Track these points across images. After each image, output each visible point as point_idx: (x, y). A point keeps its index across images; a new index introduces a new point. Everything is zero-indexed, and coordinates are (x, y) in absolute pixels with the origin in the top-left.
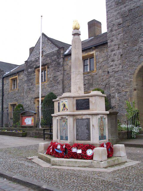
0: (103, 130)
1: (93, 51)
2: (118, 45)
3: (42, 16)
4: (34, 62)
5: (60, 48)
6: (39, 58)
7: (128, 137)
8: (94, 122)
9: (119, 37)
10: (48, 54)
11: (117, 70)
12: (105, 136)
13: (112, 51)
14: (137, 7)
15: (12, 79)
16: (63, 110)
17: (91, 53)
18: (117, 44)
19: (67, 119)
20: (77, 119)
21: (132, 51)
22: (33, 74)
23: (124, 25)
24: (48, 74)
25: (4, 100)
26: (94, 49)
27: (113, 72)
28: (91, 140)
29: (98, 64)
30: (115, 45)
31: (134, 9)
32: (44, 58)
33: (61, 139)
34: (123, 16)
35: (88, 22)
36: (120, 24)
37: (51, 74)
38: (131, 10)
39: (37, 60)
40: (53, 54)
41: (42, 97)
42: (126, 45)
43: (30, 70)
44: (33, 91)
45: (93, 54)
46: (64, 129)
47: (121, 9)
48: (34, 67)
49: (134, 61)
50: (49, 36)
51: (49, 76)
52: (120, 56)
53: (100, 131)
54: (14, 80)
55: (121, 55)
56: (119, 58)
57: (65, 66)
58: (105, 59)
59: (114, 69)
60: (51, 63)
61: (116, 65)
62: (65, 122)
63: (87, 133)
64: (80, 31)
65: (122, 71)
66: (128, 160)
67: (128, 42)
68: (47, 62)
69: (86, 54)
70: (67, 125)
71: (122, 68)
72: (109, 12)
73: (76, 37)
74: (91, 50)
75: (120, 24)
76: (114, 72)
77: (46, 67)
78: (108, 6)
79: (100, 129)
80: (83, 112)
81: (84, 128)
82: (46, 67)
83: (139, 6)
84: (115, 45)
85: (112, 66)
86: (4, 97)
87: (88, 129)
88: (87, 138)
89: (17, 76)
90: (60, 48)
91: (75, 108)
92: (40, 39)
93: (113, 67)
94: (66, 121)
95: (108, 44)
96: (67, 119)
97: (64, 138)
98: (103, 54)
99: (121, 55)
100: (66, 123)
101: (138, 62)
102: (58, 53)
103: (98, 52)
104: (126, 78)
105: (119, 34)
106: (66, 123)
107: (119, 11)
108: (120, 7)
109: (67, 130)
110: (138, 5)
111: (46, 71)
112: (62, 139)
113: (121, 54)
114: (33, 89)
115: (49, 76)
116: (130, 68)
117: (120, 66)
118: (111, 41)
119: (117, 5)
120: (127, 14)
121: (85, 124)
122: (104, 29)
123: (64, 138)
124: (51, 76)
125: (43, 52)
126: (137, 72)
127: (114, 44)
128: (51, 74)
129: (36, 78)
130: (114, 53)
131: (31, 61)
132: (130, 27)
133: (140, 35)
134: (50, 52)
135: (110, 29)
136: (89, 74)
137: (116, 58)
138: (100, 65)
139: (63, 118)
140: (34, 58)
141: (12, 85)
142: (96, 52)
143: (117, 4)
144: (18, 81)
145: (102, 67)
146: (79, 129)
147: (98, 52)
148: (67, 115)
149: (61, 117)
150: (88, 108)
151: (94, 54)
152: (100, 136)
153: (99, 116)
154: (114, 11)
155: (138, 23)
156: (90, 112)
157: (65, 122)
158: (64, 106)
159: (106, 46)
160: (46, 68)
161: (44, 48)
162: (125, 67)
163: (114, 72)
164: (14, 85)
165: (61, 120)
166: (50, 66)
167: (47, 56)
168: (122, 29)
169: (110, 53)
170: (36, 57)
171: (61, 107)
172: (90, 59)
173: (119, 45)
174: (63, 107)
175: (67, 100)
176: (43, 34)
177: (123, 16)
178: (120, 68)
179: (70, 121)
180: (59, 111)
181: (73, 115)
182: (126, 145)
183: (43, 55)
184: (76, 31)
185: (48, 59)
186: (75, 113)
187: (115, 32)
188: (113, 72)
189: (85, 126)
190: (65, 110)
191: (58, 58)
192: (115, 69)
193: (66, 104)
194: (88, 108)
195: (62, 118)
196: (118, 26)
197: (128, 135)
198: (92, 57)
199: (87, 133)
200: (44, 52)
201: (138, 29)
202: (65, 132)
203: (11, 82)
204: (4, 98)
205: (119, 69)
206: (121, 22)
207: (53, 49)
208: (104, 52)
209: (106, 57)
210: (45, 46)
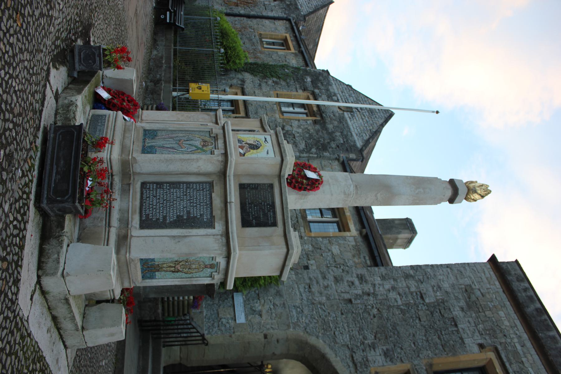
0: (173, 269)
1: (357, 230)
2: (373, 293)
3: (437, 112)
4: (328, 90)
5: (361, 151)
6: (338, 101)
7: (146, 321)
8: (202, 243)
9: (393, 295)
10: (347, 123)
11: (315, 288)
12: (152, 277)
13: (361, 278)
14: (461, 338)
15: (286, 40)
16: (240, 141)
17: (352, 226)
18: (377, 288)
19: (212, 153)
20: (211, 184)
21: (361, 329)
22: (298, 86)
23: (420, 308)
24: (299, 120)
25: (239, 18)
26: (361, 233)
27: (310, 279)
28: (142, 231)
29: (326, 241)
30: (374, 285)
31: (458, 331)
32: (337, 115)
33: (145, 130)
34: (441, 306)
35: (411, 220)
36: (422, 297)
37: (299, 127)
38: (456, 325)
39: (330, 97)
40: (346, 135)
41: (245, 101)
42: (375, 311)
43: (309, 79)
44: (260, 85)
45: (349, 230)
46: (180, 140)
47: (457, 298)
48: (317, 91)
49: (336, 333)
50: (386, 130)
51: (295, 124)
52: (347, 296)
53: (172, 262)
54: (284, 44)
55: (350, 301)
56: (343, 295)
57: (319, 162)
58: (339, 261)
59: (317, 283)
60: (327, 129)
61: (326, 287)
62: (204, 146)
63: (165, 218)
64: (460, 202)
65: (313, 304)
66: (72, 353)
67: (381, 318)
68: (328, 120)
69: (348, 214)
70: (192, 152)
71: (320, 303)
72: (449, 270)
73: (449, 193)
74: (358, 226)
75: (422, 297)
76: (308, 281)
77: (318, 118)
78: (462, 269)
79: (177, 262)
80: (233, 205)
81: (180, 207)
82: (318, 118)
83: (464, 343)
84: (374, 285)
85: (324, 278)
86: (245, 19)
87: (181, 222)
88: (147, 215)
89: (293, 50)
90: (361, 151)
91: (246, 181)
92: (378, 104)
93: (321, 281)
94: (205, 148)
95: (376, 269)
96: (212, 153)
97: (150, 143)
98: (348, 255)
99: (350, 301)
100: (198, 148)
101: (336, 342)
102: (350, 147)
103: (354, 243)
104: (294, 313)
105: (399, 294)
106: (200, 150)
107: (452, 296)
108: (460, 297)
109: (174, 153)
110: (467, 341)
111: (307, 116)
112: (145, 135)
113: (353, 300)
114: (263, 85)
115: (296, 122)
116: (320, 323)
117: (324, 298)
118: (382, 275)
119: (464, 290)
120: (446, 315)
121: (195, 213)
122: (399, 257)
123: (150, 143)
124: (295, 129)
125: (350, 110)
126: (312, 340)
127: (376, 282)
128: (299, 127)
129: (288, 93)
130: (357, 282)
131: (329, 84)
132: (417, 321)
133: (399, 347)
134: (351, 127)
135: (412, 272)
136: (300, 220)
137: (343, 286)
138: (323, 248)
139: (215, 140)
140: (336, 91)
141: (274, 39)
142: (354, 237)
143: (466, 291)
144: (281, 53)
145: (319, 250)
146: (177, 193)
147: (354, 243)
148: (226, 155)
149: (221, 136)
150: (246, 223)
151: (347, 234)
152: (153, 260)
153: (222, 262)
154: (451, 283)
155: (427, 341)
156: (235, 228)
157: (204, 146)
158: (255, 147)
159: (368, 262)
160: (314, 118)
161: (359, 116)
162: (321, 308)
163: (308, 281)
164: (273, 44)
165: (208, 135)
166: (318, 127)
167: (341, 120)
168: (412, 302)
169: (354, 271)
170: (338, 95)
171: (249, 138)
172: (337, 223)
173: (375, 295)
174: (249, 142)
175: (271, 154)
176: (388, 115)
177: (441, 304)
178: (318, 298)
179: (205, 163)
180: (233, 130)
181: (223, 174)
182: (121, 345)
183: (344, 111)
184: (462, 191)
185: (336, 123)
186: (232, 178)
187: (405, 285)
188: (310, 279)
189: (188, 213)
190: (242, 147)
191: (338, 146)
192: (315, 284)
193: (260, 154)
194: (246, 223)
195: (216, 138)
196: (418, 293)
197: (150, 321)
198: (343, 227)
199: (165, 218)
200: (350, 115)
201: (414, 343)
202: (171, 146)
203: (279, 37)
204: (242, 18)
205: (317, 294)
206: (427, 301)
207: (359, 135)
208: (354, 256)
209: (342, 262)
210: (363, 117)
